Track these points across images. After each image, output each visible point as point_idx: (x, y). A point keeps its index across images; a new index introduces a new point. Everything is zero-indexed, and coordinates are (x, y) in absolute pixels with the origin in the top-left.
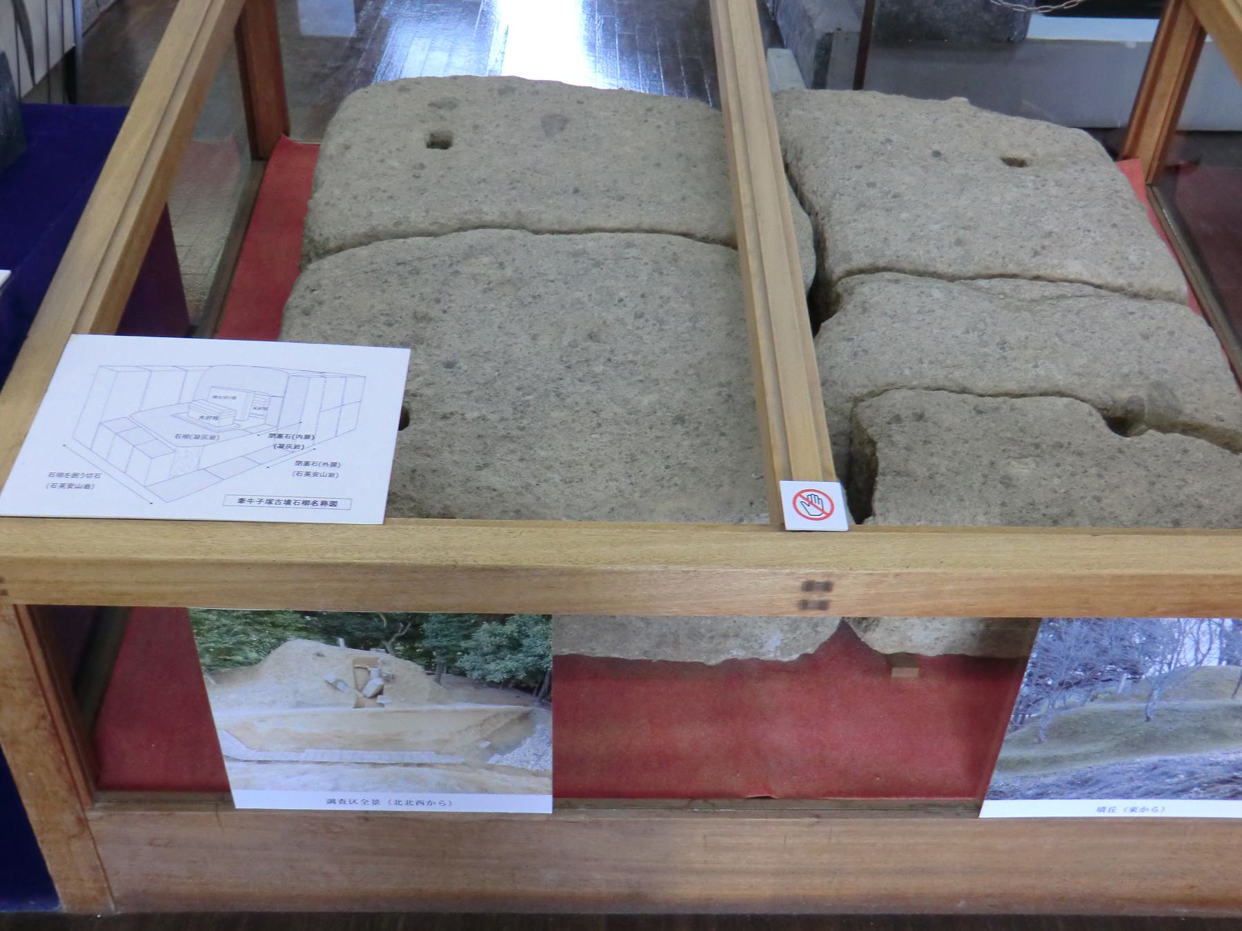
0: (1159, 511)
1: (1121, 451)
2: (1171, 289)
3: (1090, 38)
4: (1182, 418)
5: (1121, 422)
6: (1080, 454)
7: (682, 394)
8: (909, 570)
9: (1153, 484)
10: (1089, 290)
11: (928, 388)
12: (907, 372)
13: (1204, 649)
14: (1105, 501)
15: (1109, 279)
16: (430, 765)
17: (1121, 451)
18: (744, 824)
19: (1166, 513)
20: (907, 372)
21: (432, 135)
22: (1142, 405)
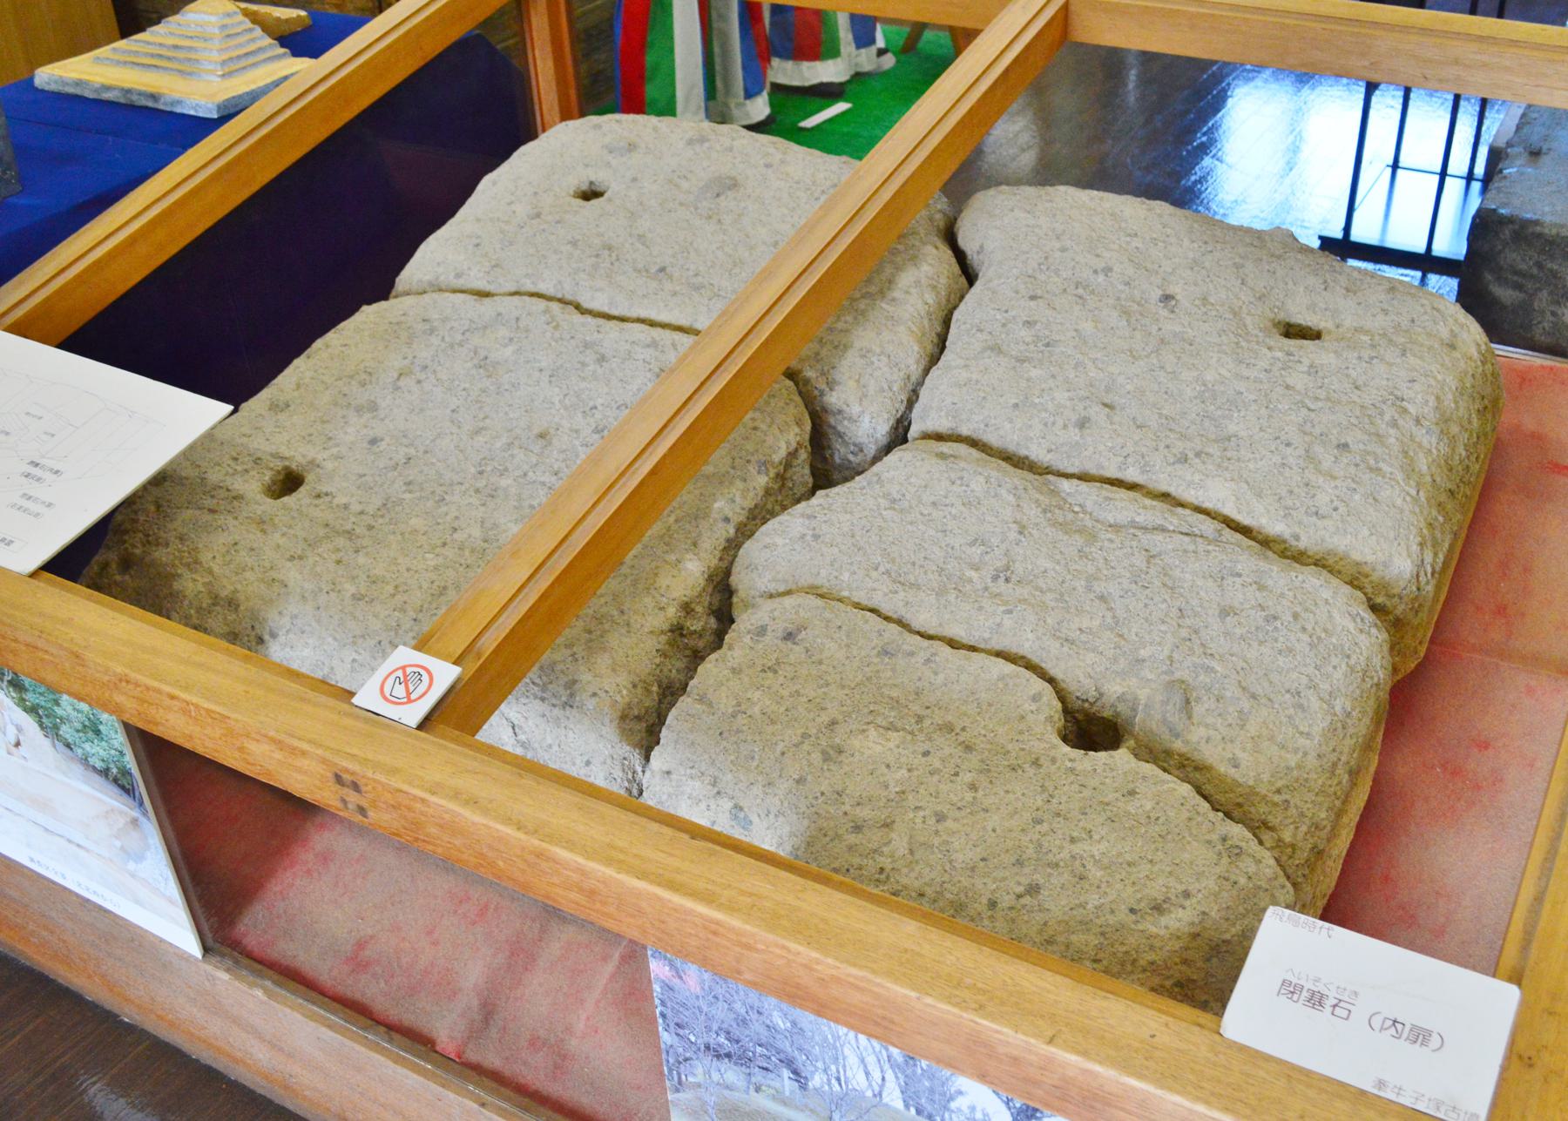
0: (1019, 863)
1: (1036, 763)
2: (1370, 558)
3: (388, 88)
4: (1178, 745)
5: (1091, 729)
6: (968, 748)
7: (1020, 571)
8: (433, 799)
9: (1039, 822)
10: (1208, 526)
11: (857, 606)
12: (846, 576)
13: (877, 1075)
14: (949, 824)
15: (1264, 521)
16: (87, 850)
17: (1036, 763)
18: (274, 1045)
19: (1026, 870)
20: (846, 576)
21: (591, 183)
22: (1134, 710)
